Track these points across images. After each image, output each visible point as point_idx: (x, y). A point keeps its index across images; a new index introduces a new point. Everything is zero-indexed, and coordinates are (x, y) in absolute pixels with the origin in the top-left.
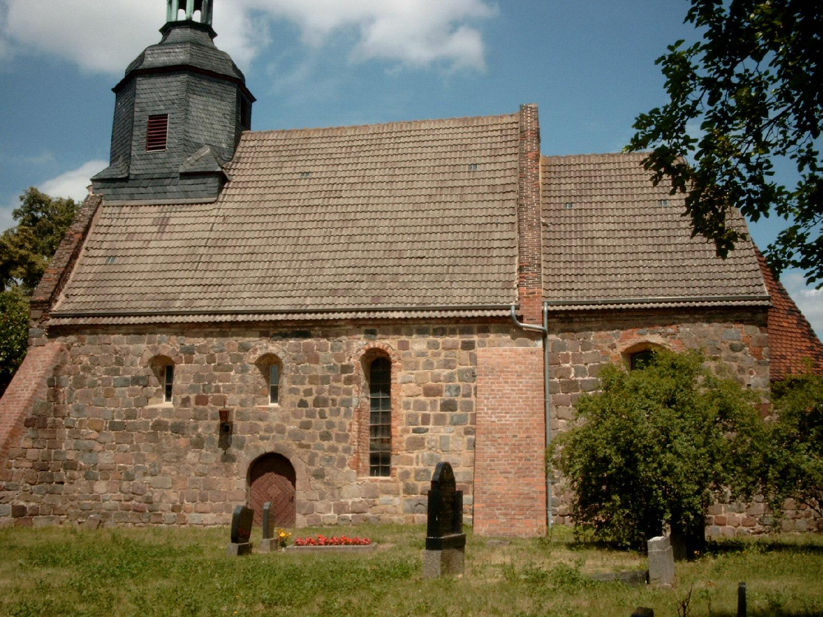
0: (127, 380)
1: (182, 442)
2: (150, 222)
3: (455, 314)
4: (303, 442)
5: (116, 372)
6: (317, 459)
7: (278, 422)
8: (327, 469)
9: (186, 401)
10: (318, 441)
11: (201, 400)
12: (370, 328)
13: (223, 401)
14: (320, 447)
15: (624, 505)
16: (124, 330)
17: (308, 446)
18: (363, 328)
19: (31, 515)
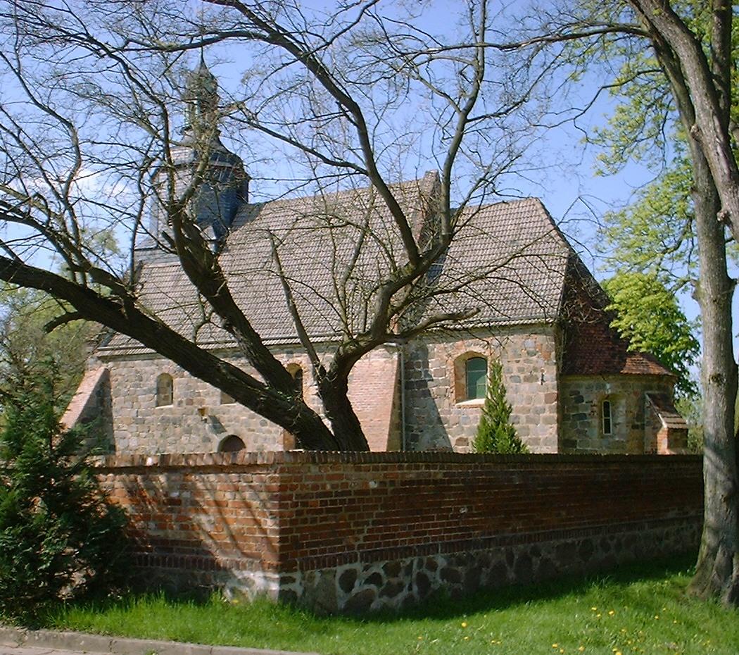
0: (144, 391)
1: (178, 430)
2: (169, 279)
3: (277, 342)
4: (251, 428)
5: (138, 386)
6: (259, 439)
7: (236, 415)
8: (265, 445)
9: (180, 403)
10: (260, 426)
11: (190, 402)
12: (289, 350)
13: (201, 402)
14: (260, 431)
15: (59, 517)
16: (142, 357)
17: (254, 430)
18: (286, 350)
19: (642, 410)
